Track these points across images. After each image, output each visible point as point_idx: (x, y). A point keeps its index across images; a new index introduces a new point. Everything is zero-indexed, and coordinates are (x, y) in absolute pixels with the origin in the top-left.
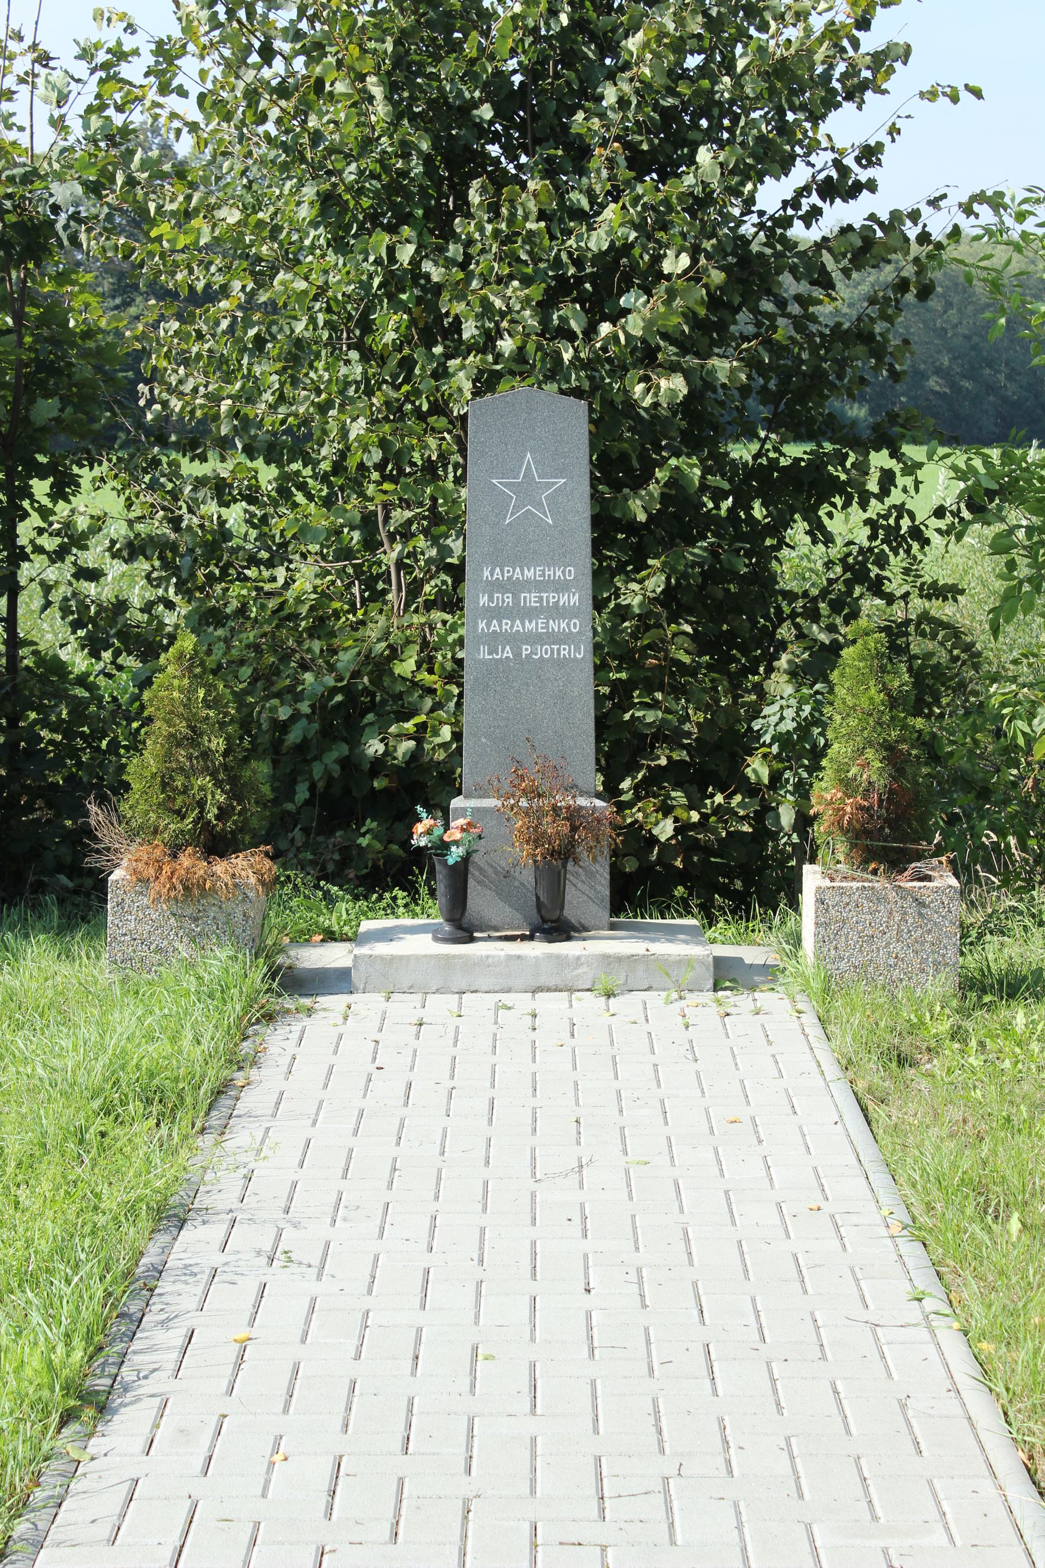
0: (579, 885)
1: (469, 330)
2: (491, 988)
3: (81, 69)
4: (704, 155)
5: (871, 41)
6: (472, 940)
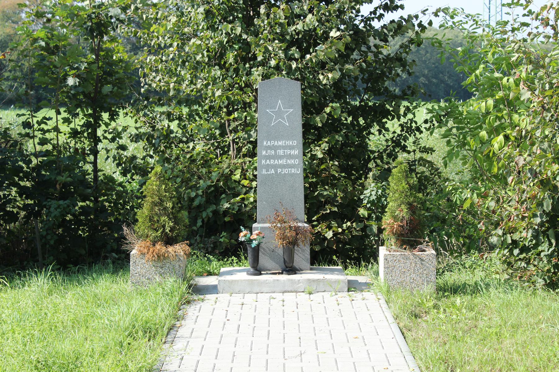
0: (299, 254)
1: (260, 58)
6: (261, 274)
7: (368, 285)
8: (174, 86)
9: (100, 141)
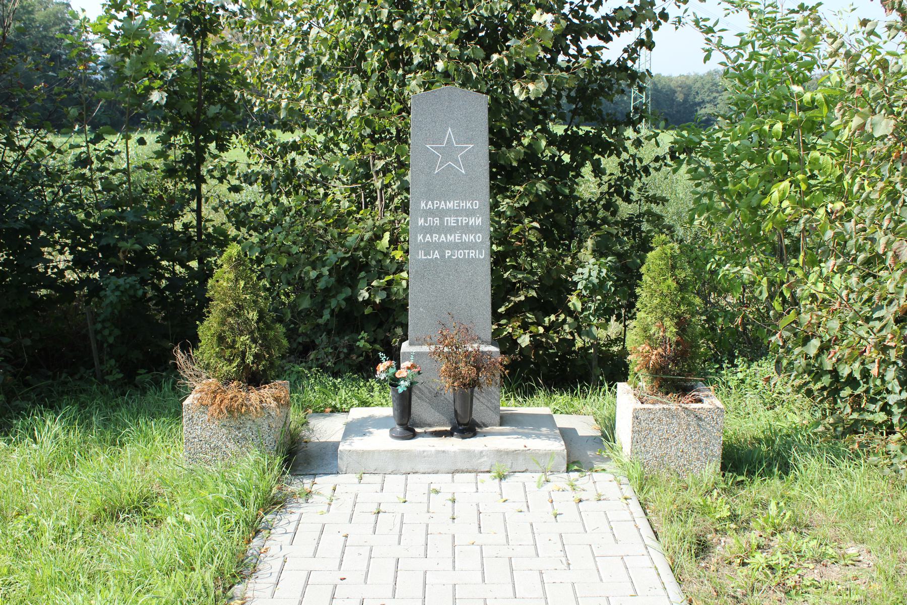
0: (481, 399)
1: (417, 59)
2: (426, 470)
6: (414, 435)
8: (288, 104)
9: (205, 181)
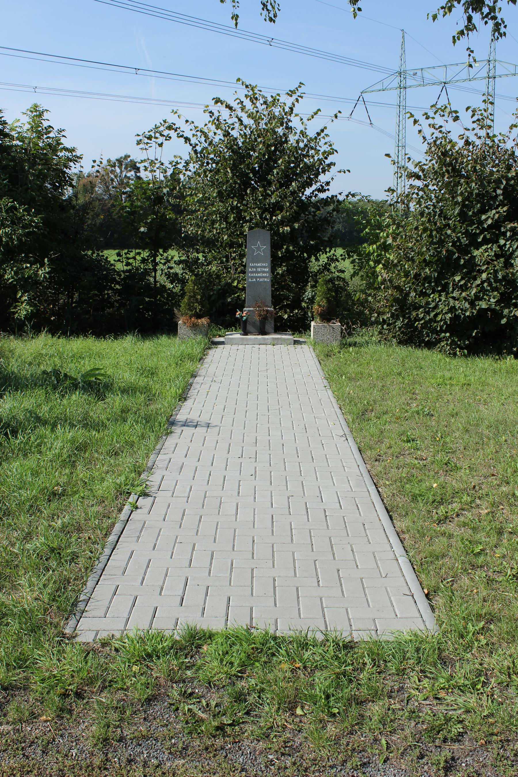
3: (170, 166)
4: (293, 184)
5: (327, 162)
7: (305, 342)
